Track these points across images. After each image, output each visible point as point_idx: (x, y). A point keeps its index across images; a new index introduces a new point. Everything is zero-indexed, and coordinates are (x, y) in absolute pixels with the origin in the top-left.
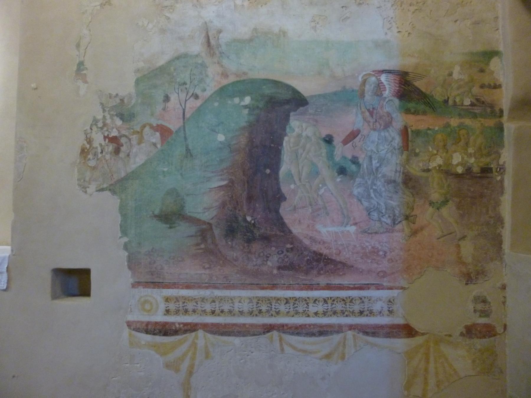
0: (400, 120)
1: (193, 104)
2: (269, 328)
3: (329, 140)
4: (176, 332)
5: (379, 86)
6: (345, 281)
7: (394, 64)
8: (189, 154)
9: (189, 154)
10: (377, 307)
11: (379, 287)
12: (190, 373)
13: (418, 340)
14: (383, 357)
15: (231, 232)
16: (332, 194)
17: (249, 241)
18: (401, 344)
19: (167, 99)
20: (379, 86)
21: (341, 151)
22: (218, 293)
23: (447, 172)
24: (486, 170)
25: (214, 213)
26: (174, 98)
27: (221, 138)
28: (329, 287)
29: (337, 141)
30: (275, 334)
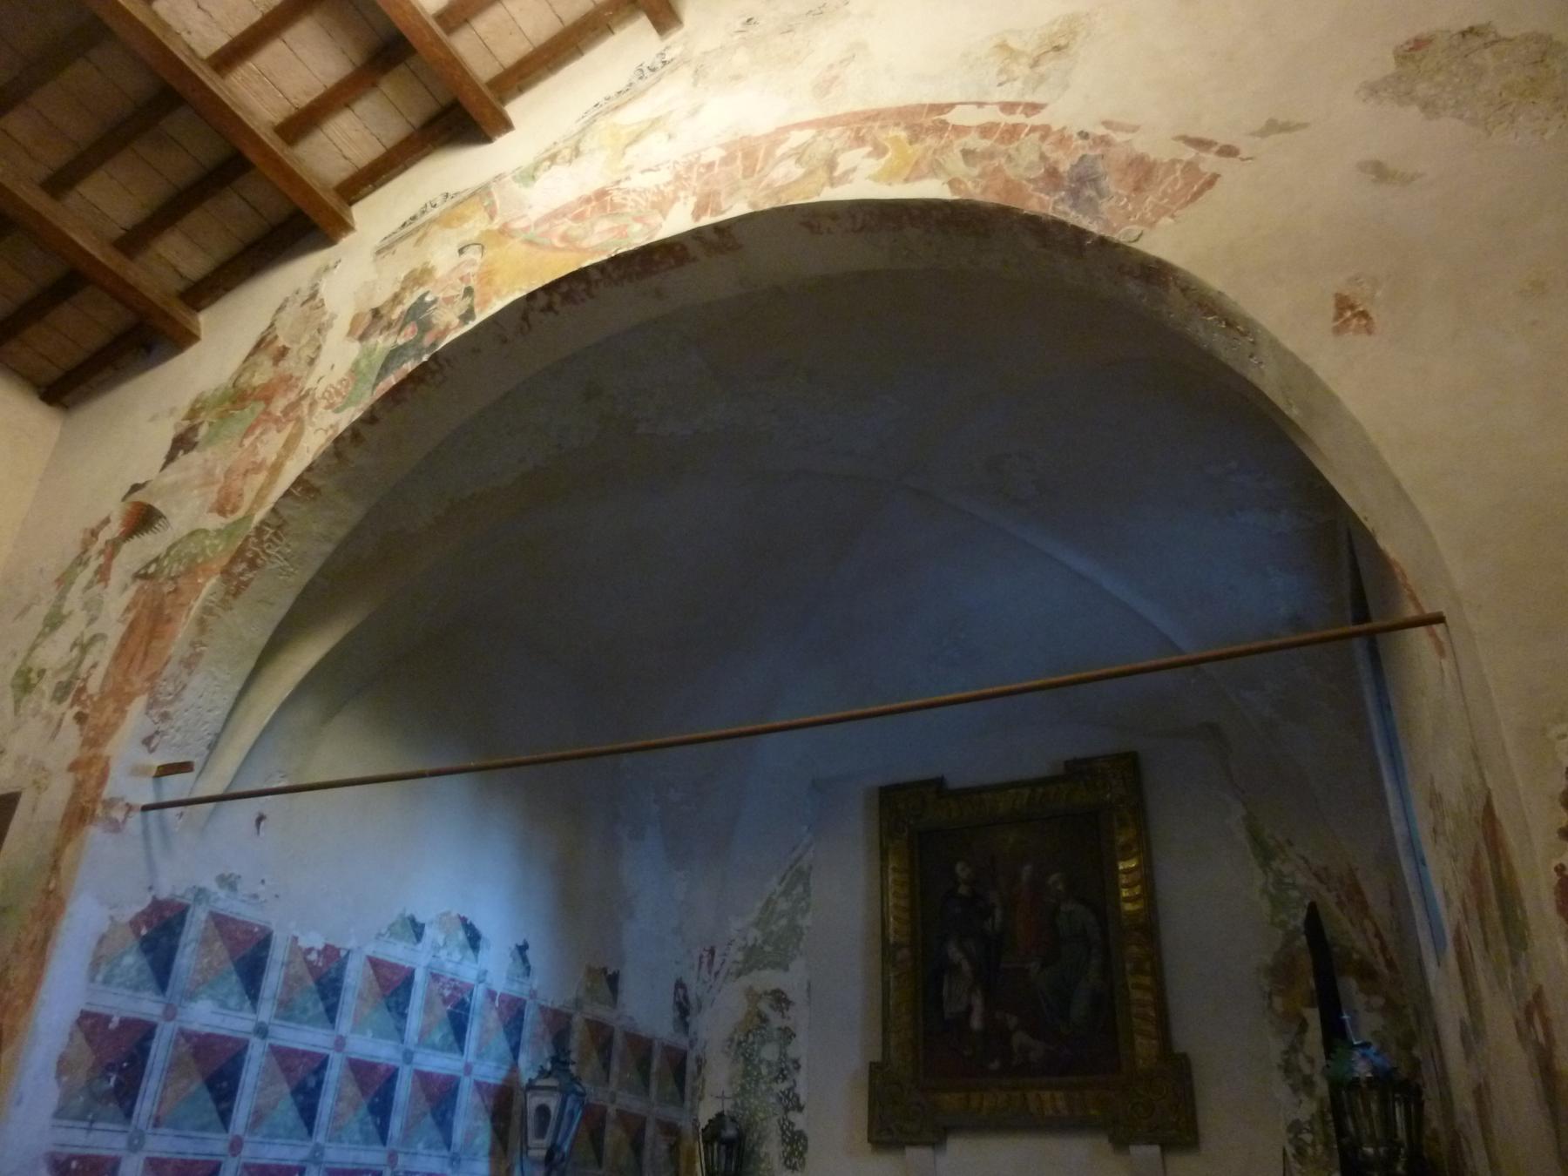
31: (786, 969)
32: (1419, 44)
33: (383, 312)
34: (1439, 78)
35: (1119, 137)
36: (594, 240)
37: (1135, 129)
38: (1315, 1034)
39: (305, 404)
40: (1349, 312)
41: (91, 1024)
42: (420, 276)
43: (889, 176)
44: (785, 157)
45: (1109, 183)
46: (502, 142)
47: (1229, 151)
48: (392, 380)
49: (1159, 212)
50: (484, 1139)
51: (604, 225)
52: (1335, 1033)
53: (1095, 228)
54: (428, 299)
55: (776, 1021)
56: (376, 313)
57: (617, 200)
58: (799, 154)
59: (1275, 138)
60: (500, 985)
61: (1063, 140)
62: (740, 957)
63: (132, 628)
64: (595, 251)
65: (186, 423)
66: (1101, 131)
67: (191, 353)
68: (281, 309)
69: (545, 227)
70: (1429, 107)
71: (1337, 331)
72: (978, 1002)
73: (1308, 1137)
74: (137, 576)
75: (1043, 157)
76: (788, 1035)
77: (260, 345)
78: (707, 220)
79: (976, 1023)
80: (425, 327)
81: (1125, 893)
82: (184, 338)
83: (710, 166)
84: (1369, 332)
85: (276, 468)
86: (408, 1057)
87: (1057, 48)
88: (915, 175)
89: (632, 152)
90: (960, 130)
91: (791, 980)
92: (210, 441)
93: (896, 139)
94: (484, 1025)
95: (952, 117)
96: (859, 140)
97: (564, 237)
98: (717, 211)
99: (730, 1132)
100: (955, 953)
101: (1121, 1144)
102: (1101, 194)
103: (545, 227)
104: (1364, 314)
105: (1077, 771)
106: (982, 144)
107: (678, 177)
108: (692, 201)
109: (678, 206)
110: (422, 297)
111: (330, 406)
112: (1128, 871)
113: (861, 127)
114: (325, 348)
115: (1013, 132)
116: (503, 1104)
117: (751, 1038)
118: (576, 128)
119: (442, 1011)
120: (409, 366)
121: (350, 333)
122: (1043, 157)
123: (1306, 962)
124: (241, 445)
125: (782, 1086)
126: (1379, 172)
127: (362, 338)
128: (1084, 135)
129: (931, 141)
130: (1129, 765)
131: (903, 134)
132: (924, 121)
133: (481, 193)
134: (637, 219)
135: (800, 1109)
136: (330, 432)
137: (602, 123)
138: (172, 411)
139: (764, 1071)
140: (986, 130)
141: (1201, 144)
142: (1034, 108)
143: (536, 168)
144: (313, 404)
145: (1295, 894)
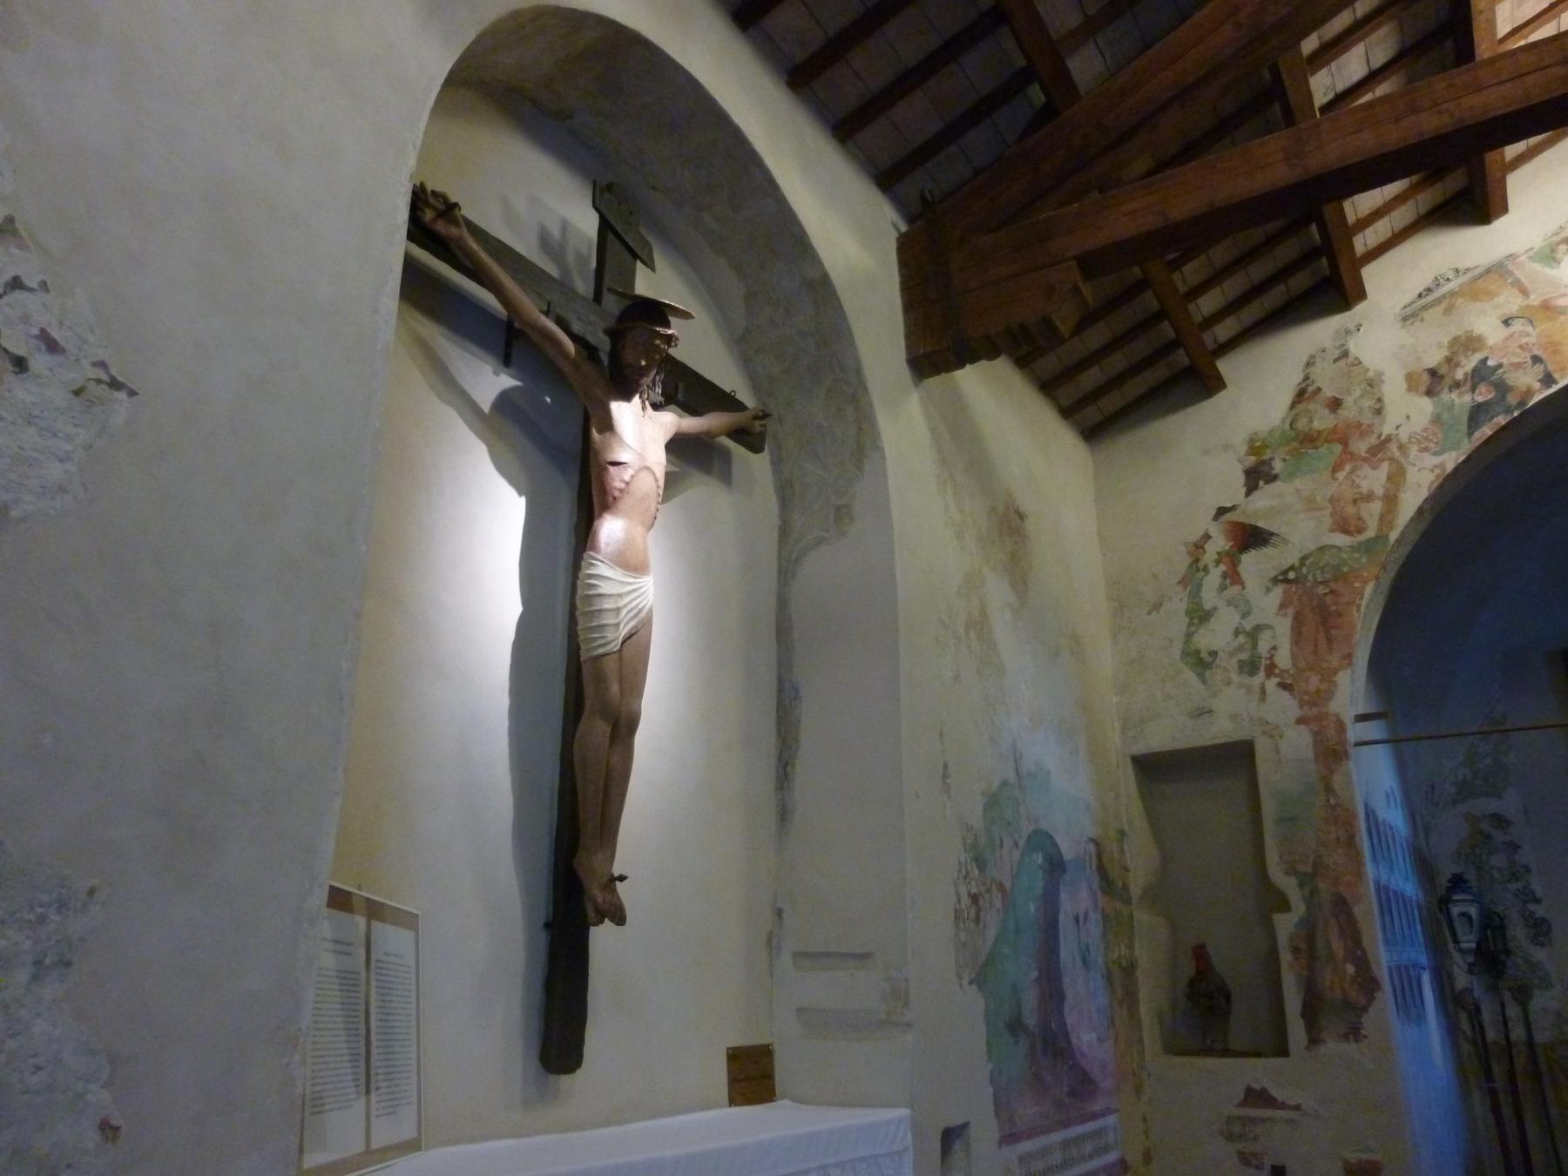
31: (1500, 797)
39: (1393, 449)
42: (1470, 343)
46: (1499, 224)
48: (1486, 431)
54: (1490, 363)
55: (1498, 836)
56: (1433, 373)
62: (1453, 790)
63: (1298, 621)
65: (1253, 459)
74: (1275, 581)
76: (1513, 847)
77: (1301, 395)
80: (1502, 388)
82: (1210, 384)
85: (1391, 500)
91: (1510, 804)
92: (1291, 476)
114: (1386, 400)
117: (1478, 851)
120: (1502, 420)
124: (1334, 479)
125: (1519, 885)
127: (1429, 393)
133: (1499, 270)
135: (1538, 901)
136: (1437, 471)
138: (1226, 448)
139: (1496, 875)
143: (1553, 251)
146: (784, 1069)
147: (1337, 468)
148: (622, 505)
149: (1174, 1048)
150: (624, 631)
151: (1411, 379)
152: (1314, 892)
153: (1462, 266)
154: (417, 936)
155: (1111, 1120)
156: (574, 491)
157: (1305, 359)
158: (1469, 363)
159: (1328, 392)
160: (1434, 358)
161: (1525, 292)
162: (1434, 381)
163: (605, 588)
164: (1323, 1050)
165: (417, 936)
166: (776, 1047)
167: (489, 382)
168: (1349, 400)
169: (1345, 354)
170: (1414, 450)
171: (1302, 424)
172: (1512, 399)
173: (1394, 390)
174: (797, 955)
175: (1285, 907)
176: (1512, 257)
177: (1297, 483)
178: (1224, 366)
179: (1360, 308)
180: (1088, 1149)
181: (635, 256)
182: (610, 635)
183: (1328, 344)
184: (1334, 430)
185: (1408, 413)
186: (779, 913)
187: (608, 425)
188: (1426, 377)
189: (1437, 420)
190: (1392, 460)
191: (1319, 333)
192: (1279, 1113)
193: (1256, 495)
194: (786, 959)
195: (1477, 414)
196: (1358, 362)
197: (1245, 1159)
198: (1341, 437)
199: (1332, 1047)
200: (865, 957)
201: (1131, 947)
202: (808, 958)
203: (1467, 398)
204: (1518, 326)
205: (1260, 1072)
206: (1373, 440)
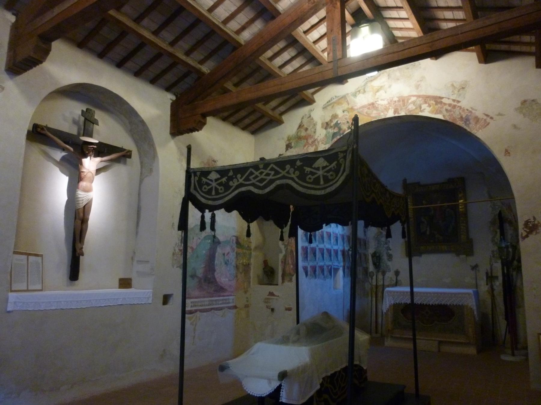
0: (236, 249)
1: (199, 241)
2: (212, 309)
3: (224, 254)
4: (221, 309)
5: (233, 240)
6: (225, 294)
7: (235, 234)
8: (197, 257)
9: (197, 257)
10: (231, 301)
11: (231, 295)
12: (196, 325)
13: (237, 309)
14: (230, 315)
15: (205, 281)
16: (195, 330)
17: (209, 283)
18: (234, 311)
19: (193, 239)
20: (233, 240)
21: (226, 258)
22: (202, 299)
23: (243, 264)
24: (249, 264)
25: (202, 275)
26: (195, 238)
27: (204, 252)
28: (224, 296)
29: (226, 254)
30: (213, 311)
32: (525, 101)
33: (329, 123)
34: (527, 109)
35: (473, 111)
36: (373, 115)
37: (476, 110)
38: (498, 234)
39: (316, 142)
40: (507, 153)
41: (302, 247)
42: (335, 116)
43: (432, 112)
44: (411, 103)
45: (471, 121)
47: (492, 118)
48: (335, 140)
49: (480, 129)
50: (342, 259)
51: (375, 112)
52: (503, 234)
53: (469, 130)
56: (327, 123)
57: (377, 105)
58: (414, 103)
59: (500, 117)
60: (341, 233)
61: (464, 110)
64: (374, 118)
65: (288, 142)
66: (470, 110)
67: (283, 126)
68: (302, 118)
69: (361, 109)
70: (524, 115)
71: (505, 155)
72: (428, 229)
73: (495, 253)
75: (460, 113)
77: (300, 126)
78: (397, 115)
79: (428, 233)
80: (340, 129)
81: (460, 207)
82: (280, 122)
83: (395, 102)
84: (510, 156)
86: (332, 247)
87: (463, 88)
88: (437, 113)
89: (378, 94)
90: (445, 104)
92: (295, 147)
93: (433, 104)
94: (340, 240)
95: (444, 101)
96: (426, 103)
97: (367, 113)
98: (398, 113)
99: (378, 255)
100: (423, 220)
101: (458, 255)
102: (470, 123)
103: (361, 109)
104: (509, 153)
105: (451, 181)
106: (449, 108)
107: (389, 103)
108: (393, 110)
109: (390, 110)
110: (337, 121)
111: (322, 143)
112: (461, 203)
113: (426, 99)
114: (317, 130)
115: (454, 107)
116: (343, 252)
118: (363, 84)
119: (335, 238)
120: (338, 137)
121: (322, 127)
122: (460, 113)
123: (498, 221)
126: (515, 127)
127: (326, 129)
128: (467, 110)
129: (439, 105)
130: (463, 180)
131: (434, 103)
132: (438, 100)
133: (344, 97)
134: (382, 112)
135: (390, 250)
137: (369, 84)
140: (450, 105)
141: (487, 116)
142: (459, 102)
143: (356, 93)
144: (318, 142)
145: (497, 207)
146: (134, 282)
147: (305, 146)
148: (85, 179)
149: (261, 283)
150: (84, 204)
151: (322, 124)
152: (287, 249)
153: (337, 95)
154: (42, 259)
155: (231, 297)
156: (76, 178)
157: (302, 117)
158: (335, 122)
159: (305, 126)
160: (328, 119)
161: (348, 104)
162: (327, 125)
163: (80, 196)
164: (284, 284)
165: (42, 259)
166: (133, 279)
167: (59, 155)
168: (309, 128)
169: (310, 116)
170: (320, 143)
171: (299, 134)
172: (341, 132)
173: (319, 127)
174: (138, 261)
175: (281, 252)
176: (348, 94)
177: (296, 149)
178: (284, 117)
179: (314, 104)
180: (221, 302)
181: (93, 123)
182: (81, 205)
183: (307, 113)
184: (305, 136)
185: (321, 133)
186: (134, 253)
187: (81, 164)
188: (325, 124)
189: (326, 135)
190: (316, 145)
191: (304, 111)
192: (275, 297)
193: (287, 151)
194: (135, 263)
195: (334, 135)
196: (312, 119)
197: (267, 307)
198: (306, 138)
199: (286, 283)
200: (148, 262)
201: (249, 259)
202: (139, 262)
203: (333, 131)
204: (346, 113)
205: (271, 288)
206: (313, 140)
